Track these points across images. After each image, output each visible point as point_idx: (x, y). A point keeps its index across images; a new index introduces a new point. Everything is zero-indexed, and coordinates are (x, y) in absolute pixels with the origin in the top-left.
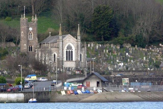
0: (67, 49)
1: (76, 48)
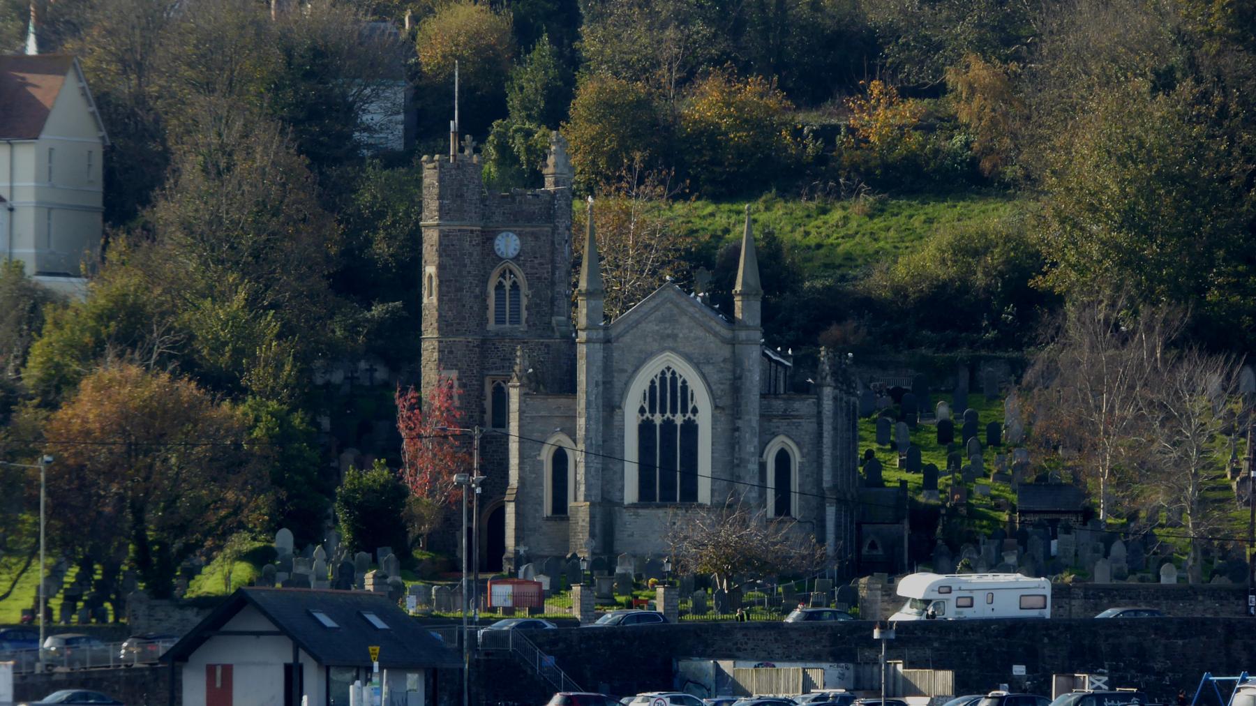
0: (652, 411)
1: (726, 401)
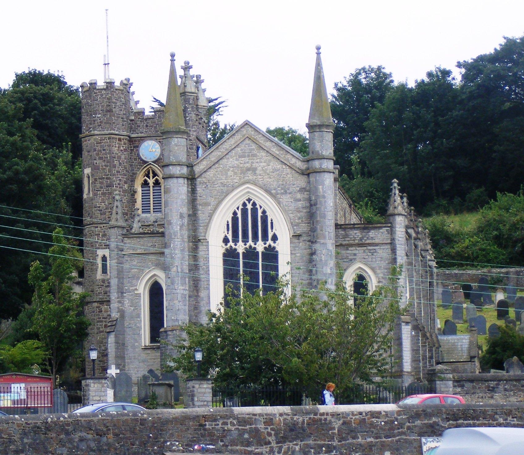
0: (235, 241)
1: (303, 228)
